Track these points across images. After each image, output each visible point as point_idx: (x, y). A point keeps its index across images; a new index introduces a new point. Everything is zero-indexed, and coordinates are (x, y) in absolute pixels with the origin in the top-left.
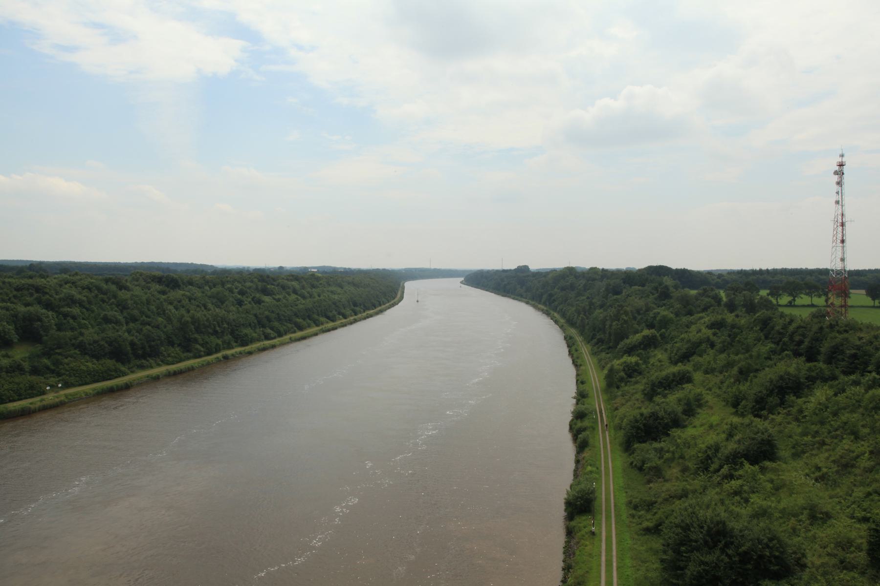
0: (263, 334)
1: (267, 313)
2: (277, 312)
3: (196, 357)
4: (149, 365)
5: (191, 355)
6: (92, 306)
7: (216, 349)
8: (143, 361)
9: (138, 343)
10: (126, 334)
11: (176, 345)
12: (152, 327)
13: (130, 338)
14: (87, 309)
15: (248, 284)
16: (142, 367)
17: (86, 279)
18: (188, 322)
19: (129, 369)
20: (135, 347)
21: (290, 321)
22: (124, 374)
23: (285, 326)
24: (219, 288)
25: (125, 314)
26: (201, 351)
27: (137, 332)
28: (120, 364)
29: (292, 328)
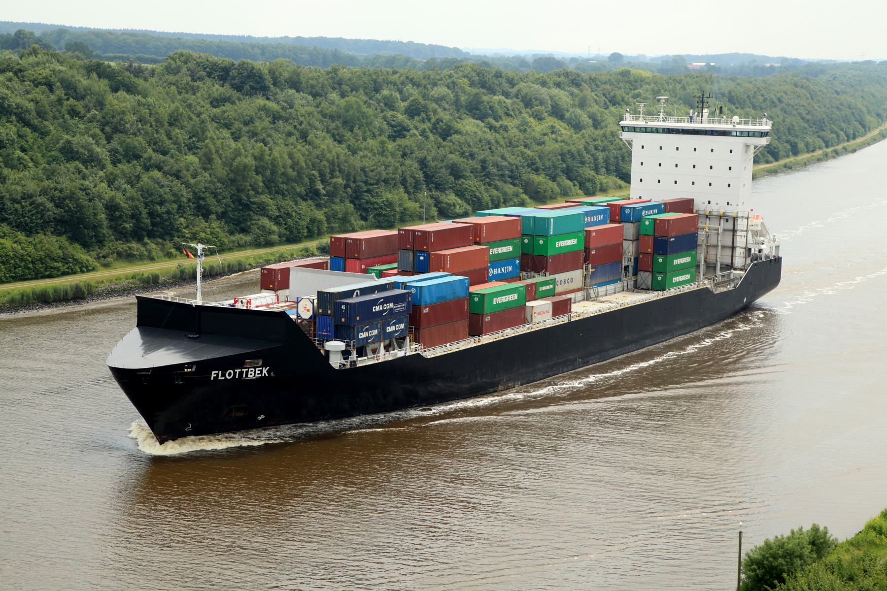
0: (436, 206)
1: (454, 158)
2: (481, 157)
3: (258, 245)
4: (146, 253)
5: (248, 238)
6: (47, 123)
7: (309, 230)
8: (134, 245)
9: (123, 205)
10: (104, 185)
11: (213, 216)
12: (165, 174)
13: (108, 193)
14: (34, 129)
15: (441, 90)
16: (129, 257)
17: (47, 65)
18: (246, 166)
19: (98, 258)
20: (117, 213)
21: (514, 178)
22: (86, 268)
23: (497, 188)
24: (356, 99)
25: (114, 144)
26: (271, 232)
27: (129, 182)
28: (77, 245)
29: (517, 195)
